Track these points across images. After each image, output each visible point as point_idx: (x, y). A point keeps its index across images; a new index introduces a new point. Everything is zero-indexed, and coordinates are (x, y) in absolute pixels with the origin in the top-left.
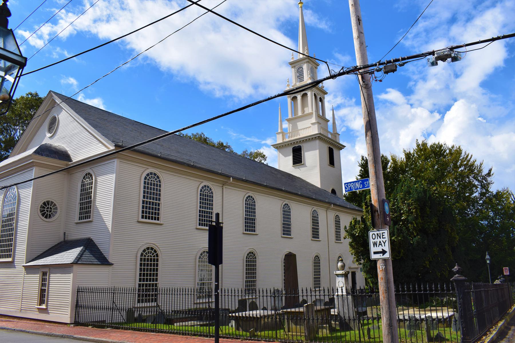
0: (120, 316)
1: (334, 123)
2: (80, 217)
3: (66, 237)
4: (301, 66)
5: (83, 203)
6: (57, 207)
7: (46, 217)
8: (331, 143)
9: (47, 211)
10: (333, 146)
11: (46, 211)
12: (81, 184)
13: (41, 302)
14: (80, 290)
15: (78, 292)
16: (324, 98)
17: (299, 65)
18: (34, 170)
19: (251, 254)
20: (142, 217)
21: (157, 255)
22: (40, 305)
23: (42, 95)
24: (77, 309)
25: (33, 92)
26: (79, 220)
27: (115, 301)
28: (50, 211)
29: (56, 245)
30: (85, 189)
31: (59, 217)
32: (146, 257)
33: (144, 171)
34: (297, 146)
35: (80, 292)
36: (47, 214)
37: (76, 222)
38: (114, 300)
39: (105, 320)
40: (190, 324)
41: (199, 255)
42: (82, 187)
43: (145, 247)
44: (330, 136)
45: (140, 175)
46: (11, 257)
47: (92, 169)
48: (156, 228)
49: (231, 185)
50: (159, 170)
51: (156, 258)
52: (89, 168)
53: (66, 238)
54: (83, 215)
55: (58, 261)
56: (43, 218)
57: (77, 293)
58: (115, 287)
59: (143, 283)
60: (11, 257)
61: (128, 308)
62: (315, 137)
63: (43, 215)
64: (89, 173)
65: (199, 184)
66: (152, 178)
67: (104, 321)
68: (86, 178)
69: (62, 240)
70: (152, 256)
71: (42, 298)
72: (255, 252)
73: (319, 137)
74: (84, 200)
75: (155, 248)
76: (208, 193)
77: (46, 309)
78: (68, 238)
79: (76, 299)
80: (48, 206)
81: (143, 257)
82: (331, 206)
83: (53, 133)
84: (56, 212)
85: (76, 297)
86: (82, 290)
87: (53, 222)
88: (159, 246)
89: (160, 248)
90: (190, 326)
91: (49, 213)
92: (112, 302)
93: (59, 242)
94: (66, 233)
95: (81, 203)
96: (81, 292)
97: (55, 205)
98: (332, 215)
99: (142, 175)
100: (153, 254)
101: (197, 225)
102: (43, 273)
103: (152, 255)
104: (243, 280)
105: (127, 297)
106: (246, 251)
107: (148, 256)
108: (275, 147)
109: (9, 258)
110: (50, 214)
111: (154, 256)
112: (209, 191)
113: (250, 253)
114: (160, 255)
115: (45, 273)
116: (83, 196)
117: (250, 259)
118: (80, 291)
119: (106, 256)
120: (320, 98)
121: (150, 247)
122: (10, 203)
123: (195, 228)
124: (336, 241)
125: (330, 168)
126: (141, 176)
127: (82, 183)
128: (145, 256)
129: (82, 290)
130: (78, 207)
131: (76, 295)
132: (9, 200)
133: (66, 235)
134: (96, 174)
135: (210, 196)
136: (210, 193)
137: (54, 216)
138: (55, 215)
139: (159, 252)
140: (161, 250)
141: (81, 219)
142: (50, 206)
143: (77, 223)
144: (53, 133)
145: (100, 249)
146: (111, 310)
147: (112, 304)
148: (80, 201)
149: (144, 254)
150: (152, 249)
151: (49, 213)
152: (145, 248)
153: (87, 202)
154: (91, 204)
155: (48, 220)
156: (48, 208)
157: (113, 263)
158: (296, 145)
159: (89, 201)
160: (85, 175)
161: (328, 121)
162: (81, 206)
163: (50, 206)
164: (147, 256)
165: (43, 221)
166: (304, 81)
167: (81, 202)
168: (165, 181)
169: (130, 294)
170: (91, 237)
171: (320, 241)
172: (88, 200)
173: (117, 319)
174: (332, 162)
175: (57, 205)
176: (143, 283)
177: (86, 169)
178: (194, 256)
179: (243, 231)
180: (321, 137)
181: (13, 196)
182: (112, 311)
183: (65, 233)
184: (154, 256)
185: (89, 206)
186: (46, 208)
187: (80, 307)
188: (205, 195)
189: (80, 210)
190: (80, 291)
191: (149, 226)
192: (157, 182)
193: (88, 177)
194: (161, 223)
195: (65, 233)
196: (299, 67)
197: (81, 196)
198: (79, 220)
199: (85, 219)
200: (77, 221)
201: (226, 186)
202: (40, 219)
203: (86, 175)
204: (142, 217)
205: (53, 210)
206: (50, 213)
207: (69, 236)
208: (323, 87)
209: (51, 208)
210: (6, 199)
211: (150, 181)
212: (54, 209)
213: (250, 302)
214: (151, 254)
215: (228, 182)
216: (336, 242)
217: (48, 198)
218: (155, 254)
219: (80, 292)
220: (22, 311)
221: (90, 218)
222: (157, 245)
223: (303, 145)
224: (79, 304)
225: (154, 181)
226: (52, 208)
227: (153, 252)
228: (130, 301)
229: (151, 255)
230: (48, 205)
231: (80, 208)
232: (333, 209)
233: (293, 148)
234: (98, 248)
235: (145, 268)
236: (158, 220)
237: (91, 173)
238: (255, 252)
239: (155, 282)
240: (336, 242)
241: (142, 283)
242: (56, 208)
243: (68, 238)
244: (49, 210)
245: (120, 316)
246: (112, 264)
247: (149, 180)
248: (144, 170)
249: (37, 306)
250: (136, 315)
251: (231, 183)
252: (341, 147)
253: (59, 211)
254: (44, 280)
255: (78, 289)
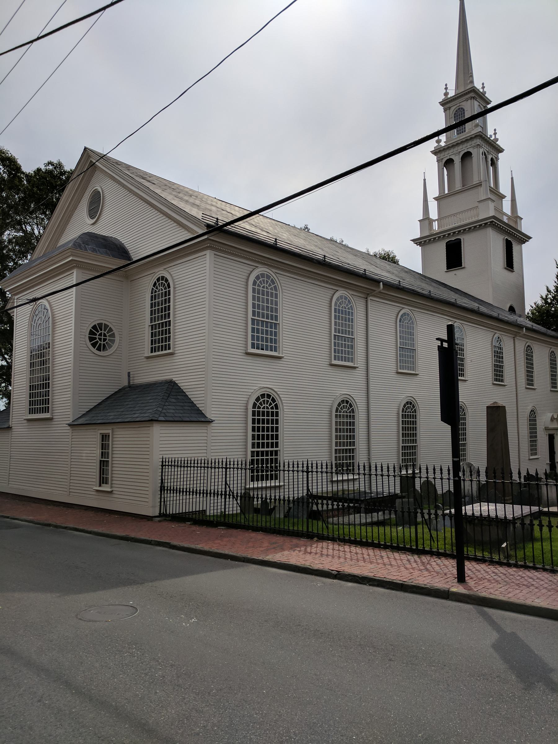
0: (235, 505)
1: (513, 200)
2: (152, 348)
3: (131, 379)
4: (460, 107)
5: (155, 325)
6: (114, 333)
7: (99, 349)
8: (509, 233)
9: (100, 339)
10: (512, 238)
11: (98, 339)
12: (150, 295)
13: (103, 480)
14: (167, 464)
15: (162, 466)
16: (497, 159)
17: (458, 105)
18: (75, 273)
19: (409, 405)
20: (253, 347)
21: (276, 406)
22: (100, 486)
23: (70, 165)
24: (163, 493)
25: (55, 161)
26: (152, 352)
27: (228, 483)
28: (105, 340)
29: (116, 392)
30: (158, 303)
31: (118, 349)
32: (261, 410)
33: (251, 272)
34: (453, 239)
35: (167, 467)
36: (100, 344)
37: (147, 355)
38: (228, 479)
39: (205, 509)
40: (357, 521)
41: (335, 406)
42: (152, 300)
43: (258, 394)
44: (505, 219)
45: (247, 275)
46: (48, 412)
47: (166, 269)
48: (272, 364)
49: (381, 296)
50: (274, 270)
51: (275, 410)
52: (162, 268)
53: (131, 382)
54: (157, 345)
55: (126, 416)
56: (94, 350)
57: (161, 467)
58: (228, 460)
59: (259, 450)
60: (48, 412)
61: (241, 493)
62: (486, 224)
63: (94, 345)
64: (163, 278)
65: (333, 293)
66: (264, 284)
67: (203, 510)
68: (159, 284)
69: (126, 384)
70: (270, 407)
71: (103, 474)
72: (356, 406)
73: (491, 222)
74: (158, 320)
75: (273, 394)
76: (345, 308)
77: (111, 492)
78: (135, 381)
79: (160, 478)
80: (100, 332)
81: (256, 410)
82: (523, 331)
83: (97, 217)
84: (113, 341)
85: (160, 474)
86: (170, 464)
87: (114, 354)
88: (278, 393)
89: (281, 396)
90: (358, 525)
91: (102, 343)
92: (224, 483)
93: (120, 388)
94: (131, 373)
95: (152, 326)
96: (168, 466)
97: (111, 330)
98: (521, 345)
99: (250, 274)
100: (271, 404)
101: (246, 347)
102: (103, 436)
103: (270, 405)
104: (399, 445)
105: (235, 475)
106: (403, 398)
107: (264, 408)
108: (416, 243)
109: (45, 412)
110: (104, 344)
111: (272, 408)
112: (347, 305)
113: (407, 403)
114: (280, 406)
115: (106, 435)
116: (155, 314)
117: (408, 412)
118: (165, 466)
119: (201, 409)
120: (492, 159)
121: (266, 393)
122: (40, 329)
123: (328, 363)
124: (528, 386)
125: (507, 273)
126: (248, 277)
127: (152, 293)
128: (260, 408)
129: (170, 464)
130: (147, 332)
131: (160, 470)
132: (38, 324)
133: (131, 376)
134: (175, 278)
135: (349, 312)
136: (349, 309)
137: (110, 347)
138: (112, 346)
139: (278, 401)
140: (282, 399)
141: (155, 351)
142: (103, 332)
143: (148, 358)
144: (97, 217)
145: (190, 397)
146: (223, 496)
147: (224, 487)
148: (151, 322)
149: (258, 404)
150: (269, 396)
151: (102, 343)
152: (259, 395)
153: (162, 323)
154: (170, 325)
155: (102, 353)
156: (100, 335)
157: (213, 419)
158: (451, 237)
159: (166, 322)
160: (156, 280)
161: (502, 197)
162: (152, 330)
163: (103, 332)
164: (262, 407)
165: (93, 355)
166: (465, 131)
167: (153, 323)
168: (283, 288)
169: (296, 474)
170: (174, 379)
171: (505, 385)
172: (164, 321)
173: (216, 508)
174: (509, 264)
175: (115, 331)
176: (259, 450)
177: (156, 270)
178: (397, 405)
179: (397, 369)
180: (496, 223)
181: (44, 317)
182: (225, 498)
183: (129, 373)
184: (272, 408)
185: (166, 330)
186: (98, 334)
187: (167, 490)
188: (342, 310)
189: (152, 337)
190: (165, 466)
191: (269, 361)
192: (271, 289)
193: (162, 283)
194: (280, 355)
195: (129, 373)
196: (457, 109)
197: (151, 315)
198: (152, 352)
199: (162, 350)
200: (148, 353)
201: (371, 298)
202: (90, 352)
203: (158, 280)
204: (253, 347)
205: (108, 338)
206: (105, 343)
207: (135, 378)
208: (497, 140)
209: (105, 335)
210: (33, 323)
211: (261, 288)
212: (109, 336)
213: (422, 482)
214: (267, 404)
215: (375, 291)
216: (526, 388)
217: (98, 318)
218: (273, 405)
219: (167, 467)
220: (71, 493)
221: (169, 349)
222: (276, 390)
223: (463, 237)
224: (166, 485)
225: (267, 288)
226: (107, 335)
227: (270, 400)
228: (239, 478)
229: (268, 406)
230: (101, 330)
231: (152, 333)
232: (525, 336)
233: (446, 243)
234: (187, 396)
235: (274, 427)
236: (276, 351)
237: (165, 276)
238: (356, 406)
239: (275, 449)
240: (526, 388)
241: (256, 449)
242: (113, 335)
243: (135, 381)
244: (102, 337)
245: (235, 505)
246: (210, 422)
247: (260, 287)
248: (251, 270)
249: (96, 487)
250: (257, 503)
251: (380, 292)
252: (524, 239)
253: (117, 339)
254: (104, 447)
255: (162, 462)
